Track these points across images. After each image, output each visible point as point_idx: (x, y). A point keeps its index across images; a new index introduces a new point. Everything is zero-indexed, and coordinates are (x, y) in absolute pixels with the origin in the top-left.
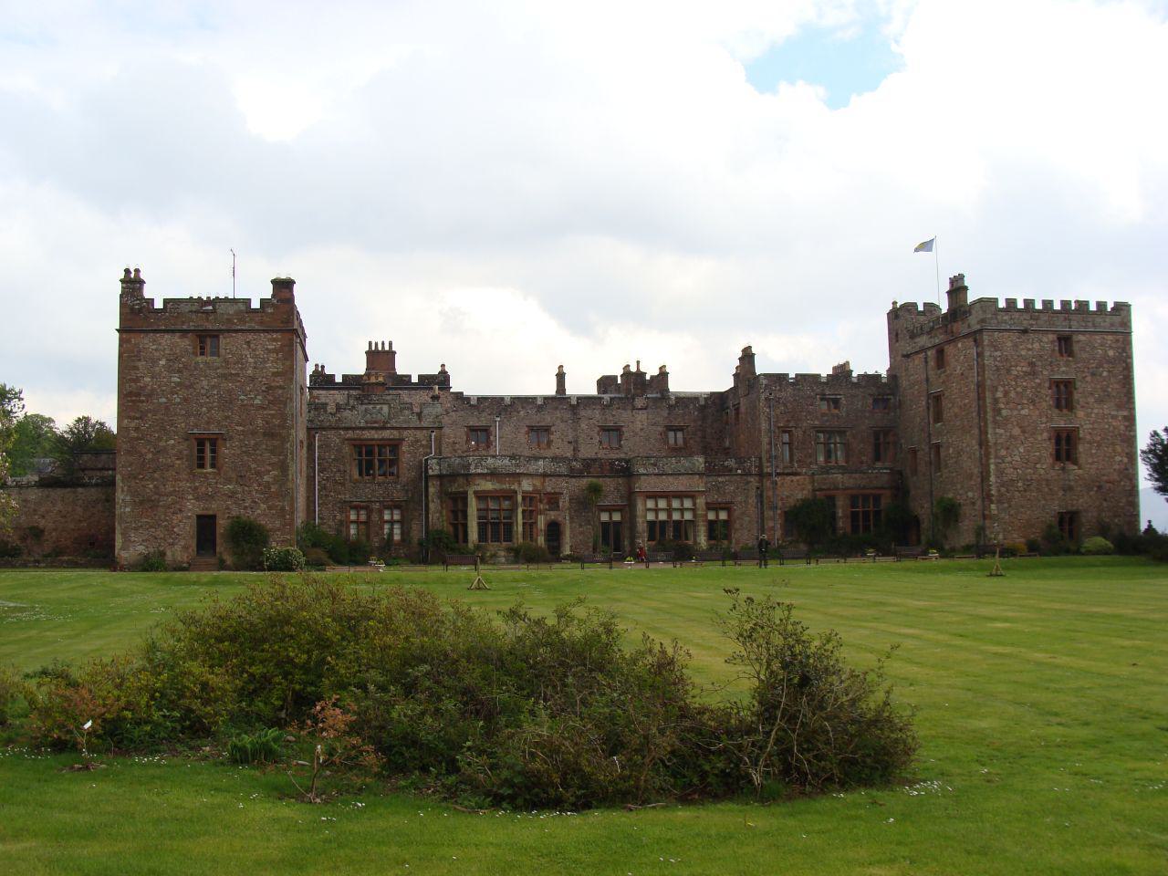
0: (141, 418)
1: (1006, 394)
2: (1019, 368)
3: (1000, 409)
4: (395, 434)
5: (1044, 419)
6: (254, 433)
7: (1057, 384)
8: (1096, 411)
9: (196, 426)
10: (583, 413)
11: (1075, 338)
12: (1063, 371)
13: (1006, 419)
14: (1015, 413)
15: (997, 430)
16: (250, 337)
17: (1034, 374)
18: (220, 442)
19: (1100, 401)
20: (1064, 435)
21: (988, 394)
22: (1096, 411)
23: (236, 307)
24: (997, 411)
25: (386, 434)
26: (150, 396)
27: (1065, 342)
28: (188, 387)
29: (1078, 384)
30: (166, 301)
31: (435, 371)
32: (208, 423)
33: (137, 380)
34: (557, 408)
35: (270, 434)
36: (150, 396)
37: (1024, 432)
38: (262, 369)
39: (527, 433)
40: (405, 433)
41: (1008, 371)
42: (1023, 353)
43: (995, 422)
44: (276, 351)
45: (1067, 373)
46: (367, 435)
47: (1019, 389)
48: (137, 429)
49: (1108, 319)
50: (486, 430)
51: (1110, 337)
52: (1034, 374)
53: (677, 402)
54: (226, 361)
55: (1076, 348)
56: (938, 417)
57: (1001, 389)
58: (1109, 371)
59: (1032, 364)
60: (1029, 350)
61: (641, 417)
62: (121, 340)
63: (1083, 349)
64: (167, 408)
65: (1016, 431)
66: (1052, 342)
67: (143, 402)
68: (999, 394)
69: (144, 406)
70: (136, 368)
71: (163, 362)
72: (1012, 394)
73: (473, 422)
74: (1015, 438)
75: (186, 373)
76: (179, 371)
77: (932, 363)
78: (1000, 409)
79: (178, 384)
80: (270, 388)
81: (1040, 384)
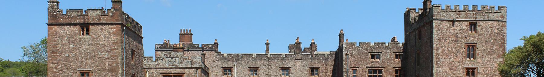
0: (57, 63)
1: (443, 51)
2: (450, 39)
3: (440, 59)
4: (181, 71)
5: (461, 63)
6: (104, 70)
7: (469, 46)
8: (486, 59)
9: (80, 66)
10: (273, 61)
11: (478, 23)
12: (471, 41)
13: (443, 63)
14: (447, 60)
15: (438, 69)
16: (103, 27)
17: (457, 41)
18: (90, 74)
19: (489, 54)
20: (471, 71)
21: (434, 51)
22: (486, 59)
23: (96, 13)
24: (439, 59)
25: (177, 71)
26: (61, 53)
27: (473, 26)
28: (77, 50)
29: (478, 46)
30: (67, 11)
31: (212, 42)
32: (85, 65)
33: (55, 46)
34: (261, 59)
35: (111, 71)
36: (61, 53)
37: (451, 69)
38: (108, 41)
39: (248, 70)
40: (186, 70)
41: (445, 40)
42: (452, 31)
43: (437, 64)
44: (113, 33)
45: (473, 40)
46: (169, 71)
47: (450, 49)
48: (56, 68)
49: (495, 15)
50: (230, 69)
51: (495, 23)
52: (457, 41)
53: (286, 57)
54: (92, 38)
55: (478, 29)
56: (419, 64)
57: (440, 49)
58: (494, 40)
59: (456, 36)
60: (455, 30)
61: (299, 63)
62: (48, 28)
63: (482, 29)
64: (68, 59)
65: (447, 69)
66: (467, 26)
67: (58, 56)
68: (440, 51)
69: (59, 58)
70: (55, 41)
71: (66, 38)
72: (446, 51)
73: (226, 65)
74: (446, 72)
75: (76, 43)
76: (73, 42)
77: (417, 37)
78: (440, 59)
79: (73, 48)
80: (111, 50)
81: (459, 47)
